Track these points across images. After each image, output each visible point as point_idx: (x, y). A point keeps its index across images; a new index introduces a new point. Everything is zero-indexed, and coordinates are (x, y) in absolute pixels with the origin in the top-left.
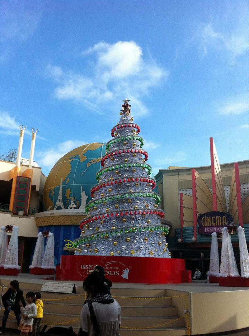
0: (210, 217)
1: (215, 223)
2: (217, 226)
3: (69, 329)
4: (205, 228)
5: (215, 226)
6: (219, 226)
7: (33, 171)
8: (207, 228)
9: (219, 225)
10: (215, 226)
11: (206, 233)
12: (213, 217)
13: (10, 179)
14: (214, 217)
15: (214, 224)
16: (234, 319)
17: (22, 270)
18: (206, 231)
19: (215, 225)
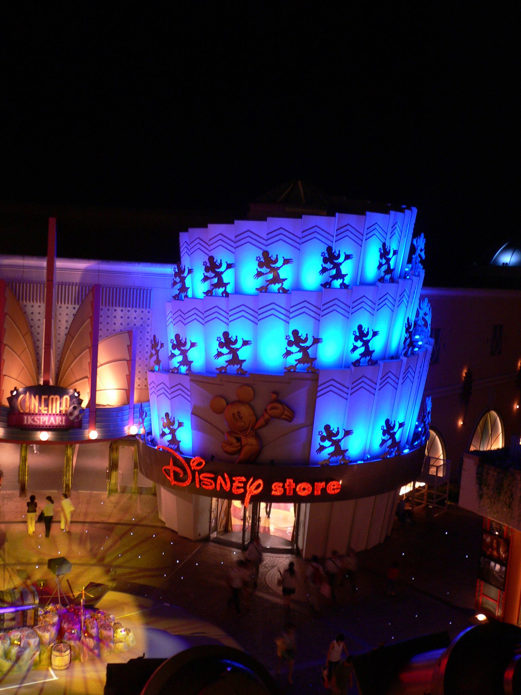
0: (37, 397)
1: (46, 408)
2: (50, 415)
3: (281, 579)
4: (25, 417)
5: (47, 415)
6: (54, 415)
7: (289, 423)
8: (29, 417)
9: (54, 412)
10: (47, 415)
11: (26, 425)
12: (43, 397)
13: (40, 513)
14: (46, 397)
15: (45, 410)
16: (241, 525)
17: (169, 661)
18: (25, 422)
19: (46, 412)
